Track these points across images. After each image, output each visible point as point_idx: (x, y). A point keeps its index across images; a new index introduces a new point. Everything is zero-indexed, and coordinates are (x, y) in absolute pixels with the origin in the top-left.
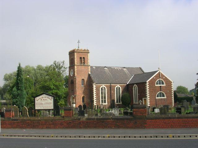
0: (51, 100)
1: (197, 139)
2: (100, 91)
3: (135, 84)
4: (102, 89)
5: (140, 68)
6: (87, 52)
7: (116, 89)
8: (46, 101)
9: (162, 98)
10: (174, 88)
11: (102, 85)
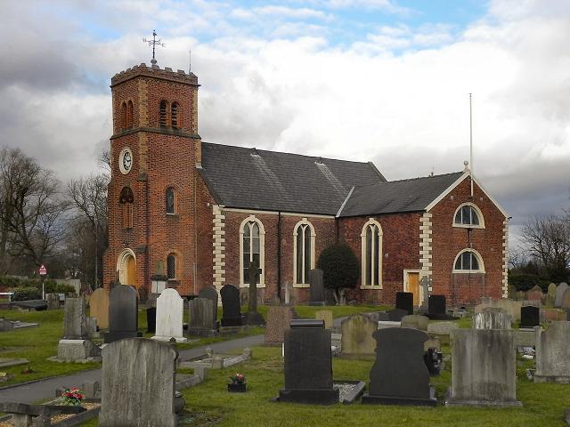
4: (299, 230)
7: (295, 233)
9: (472, 271)
11: (248, 215)
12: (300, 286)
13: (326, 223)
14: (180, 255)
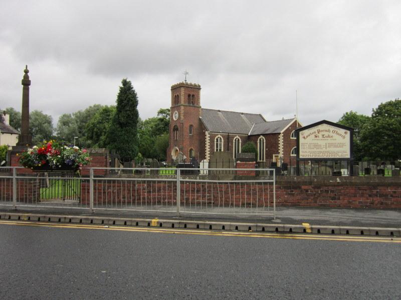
0: (344, 137)
2: (215, 143)
3: (261, 135)
5: (260, 115)
6: (197, 88)
7: (234, 141)
8: (329, 141)
11: (218, 135)
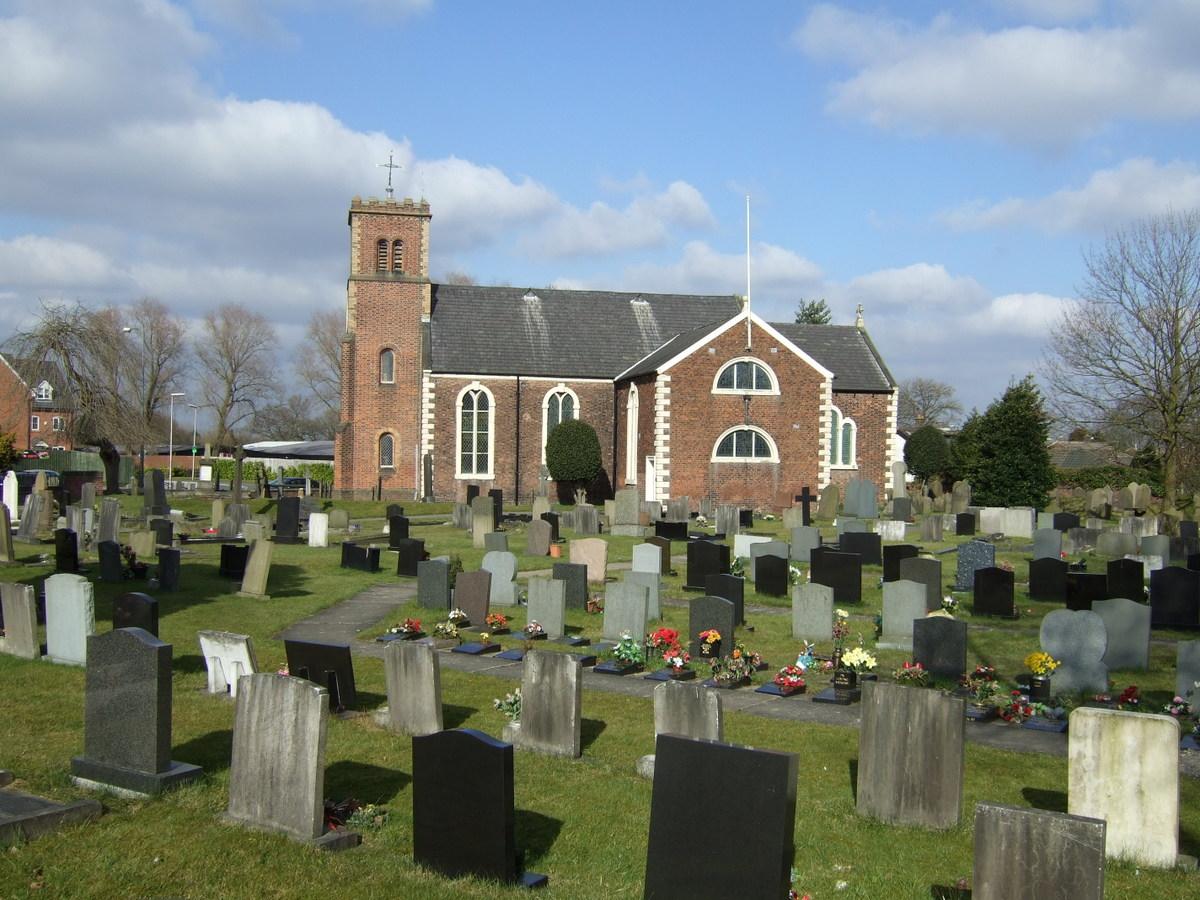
1: (1185, 227)
4: (467, 399)
7: (545, 405)
9: (754, 460)
10: (180, 340)
11: (470, 382)
12: (466, 476)
13: (599, 390)
14: (397, 434)
